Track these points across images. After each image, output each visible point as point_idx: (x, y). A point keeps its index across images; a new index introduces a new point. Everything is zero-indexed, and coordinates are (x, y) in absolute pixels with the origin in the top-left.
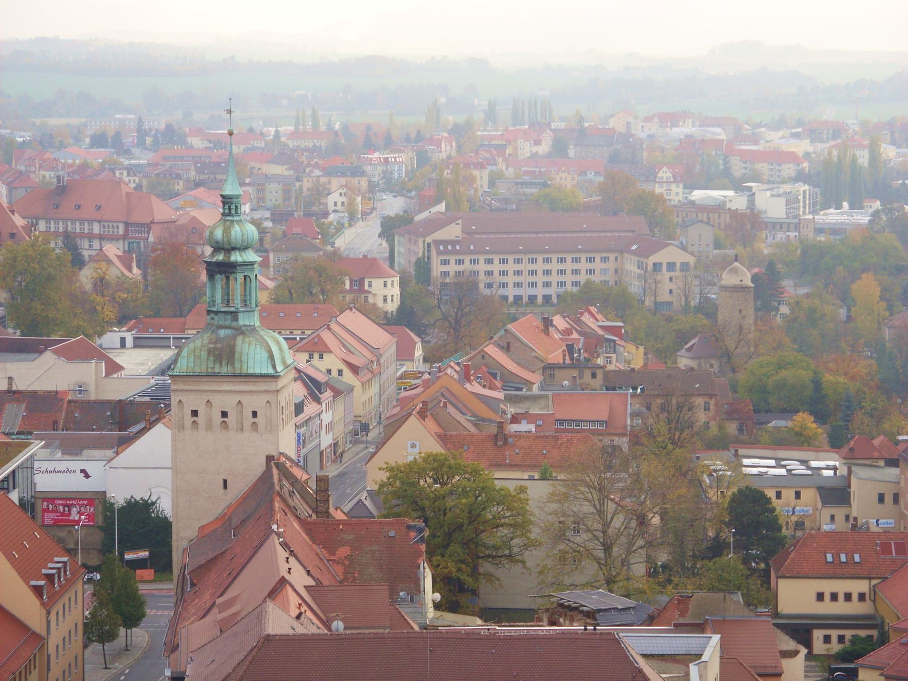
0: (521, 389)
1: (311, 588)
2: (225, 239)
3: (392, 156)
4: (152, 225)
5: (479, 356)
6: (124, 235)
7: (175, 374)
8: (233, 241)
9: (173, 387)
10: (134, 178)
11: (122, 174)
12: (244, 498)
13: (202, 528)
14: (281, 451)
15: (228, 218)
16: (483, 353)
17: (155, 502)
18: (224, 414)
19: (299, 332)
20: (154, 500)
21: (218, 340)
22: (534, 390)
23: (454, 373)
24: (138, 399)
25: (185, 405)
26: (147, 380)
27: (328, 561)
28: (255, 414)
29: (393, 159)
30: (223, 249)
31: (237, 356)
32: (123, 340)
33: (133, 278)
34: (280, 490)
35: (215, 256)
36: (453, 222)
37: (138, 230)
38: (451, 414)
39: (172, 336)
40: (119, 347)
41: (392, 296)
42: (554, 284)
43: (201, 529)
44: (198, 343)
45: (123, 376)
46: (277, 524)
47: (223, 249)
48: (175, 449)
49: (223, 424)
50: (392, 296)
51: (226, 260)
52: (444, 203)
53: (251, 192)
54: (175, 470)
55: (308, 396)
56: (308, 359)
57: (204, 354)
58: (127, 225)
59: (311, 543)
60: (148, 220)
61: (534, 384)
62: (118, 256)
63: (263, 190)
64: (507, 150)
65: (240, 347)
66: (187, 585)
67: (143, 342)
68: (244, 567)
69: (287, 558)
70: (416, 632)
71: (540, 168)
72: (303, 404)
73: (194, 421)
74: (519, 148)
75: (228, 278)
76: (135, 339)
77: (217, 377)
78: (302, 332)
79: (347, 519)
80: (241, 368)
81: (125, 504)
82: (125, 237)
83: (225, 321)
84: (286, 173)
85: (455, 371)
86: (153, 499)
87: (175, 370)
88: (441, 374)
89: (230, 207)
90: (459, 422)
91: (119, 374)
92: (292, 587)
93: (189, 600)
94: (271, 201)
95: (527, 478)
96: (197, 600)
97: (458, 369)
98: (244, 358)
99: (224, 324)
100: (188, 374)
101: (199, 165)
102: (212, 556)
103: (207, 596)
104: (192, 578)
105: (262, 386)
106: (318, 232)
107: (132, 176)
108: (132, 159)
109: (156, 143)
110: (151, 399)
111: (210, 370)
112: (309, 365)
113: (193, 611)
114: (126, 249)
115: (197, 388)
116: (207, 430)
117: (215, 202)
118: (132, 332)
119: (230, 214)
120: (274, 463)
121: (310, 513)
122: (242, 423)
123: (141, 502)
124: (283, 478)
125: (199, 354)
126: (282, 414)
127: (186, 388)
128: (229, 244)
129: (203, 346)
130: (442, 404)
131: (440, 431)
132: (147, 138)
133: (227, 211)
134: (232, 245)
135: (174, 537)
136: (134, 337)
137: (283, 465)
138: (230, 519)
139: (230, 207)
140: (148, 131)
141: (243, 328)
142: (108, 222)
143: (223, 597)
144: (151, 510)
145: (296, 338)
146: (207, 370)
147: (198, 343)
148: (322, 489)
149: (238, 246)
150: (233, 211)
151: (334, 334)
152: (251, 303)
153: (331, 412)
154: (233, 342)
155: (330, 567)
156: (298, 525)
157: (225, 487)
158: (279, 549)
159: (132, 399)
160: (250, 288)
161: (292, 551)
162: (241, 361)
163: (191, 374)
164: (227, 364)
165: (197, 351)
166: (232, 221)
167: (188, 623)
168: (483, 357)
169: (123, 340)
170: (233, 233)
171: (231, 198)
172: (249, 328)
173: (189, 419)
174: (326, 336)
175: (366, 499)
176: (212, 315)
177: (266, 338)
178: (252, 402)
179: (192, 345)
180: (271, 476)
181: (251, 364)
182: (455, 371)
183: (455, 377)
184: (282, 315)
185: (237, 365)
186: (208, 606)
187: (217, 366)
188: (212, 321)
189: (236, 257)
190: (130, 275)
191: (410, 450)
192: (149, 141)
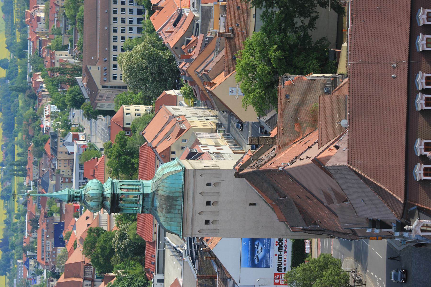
0: (198, 24)
2: (97, 200)
3: (45, 113)
5: (176, 50)
6: (92, 281)
9: (190, 236)
13: (280, 219)
15: (83, 198)
16: (174, 48)
18: (208, 203)
21: (161, 206)
22: (199, 16)
23: (186, 66)
28: (209, 184)
29: (47, 112)
30: (102, 202)
31: (171, 195)
35: (107, 207)
36: (89, 71)
38: (212, 67)
39: (157, 250)
41: (135, 110)
42: (131, 7)
43: (281, 220)
45: (182, 279)
49: (214, 204)
50: (135, 110)
52: (76, 78)
57: (170, 215)
61: (194, 16)
64: (43, 39)
66: (315, 227)
67: (161, 270)
69: (300, 159)
70: (349, 80)
71: (55, 18)
73: (212, 222)
74: (42, 31)
75: (121, 200)
76: (158, 273)
79: (277, 128)
80: (179, 192)
83: (148, 202)
85: (185, 65)
87: (179, 234)
88: (187, 74)
90: (218, 62)
95: (254, 19)
97: (184, 63)
98: (173, 190)
99: (150, 203)
101: (48, 236)
106: (93, 158)
111: (180, 212)
114: (101, 280)
117: (71, 226)
118: (154, 275)
120: (240, 172)
121: (272, 149)
125: (170, 219)
126: (209, 167)
127: (190, 228)
128: (99, 197)
130: (206, 73)
131: (223, 74)
133: (78, 199)
134: (101, 195)
138: (275, 201)
139: (76, 197)
143: (324, 202)
146: (179, 214)
148: (258, 141)
150: (79, 194)
151: (158, 144)
153: (208, 147)
156: (280, 156)
157: (255, 204)
158: (295, 165)
160: (128, 185)
162: (174, 192)
164: (176, 201)
168: (176, 48)
174: (160, 150)
175: (265, 119)
176: (145, 210)
177: (160, 176)
178: (201, 186)
180: (248, 173)
181: (176, 186)
182: (185, 65)
183: (189, 65)
185: (177, 194)
186: (328, 212)
187: (177, 207)
188: (149, 210)
191: (235, 93)
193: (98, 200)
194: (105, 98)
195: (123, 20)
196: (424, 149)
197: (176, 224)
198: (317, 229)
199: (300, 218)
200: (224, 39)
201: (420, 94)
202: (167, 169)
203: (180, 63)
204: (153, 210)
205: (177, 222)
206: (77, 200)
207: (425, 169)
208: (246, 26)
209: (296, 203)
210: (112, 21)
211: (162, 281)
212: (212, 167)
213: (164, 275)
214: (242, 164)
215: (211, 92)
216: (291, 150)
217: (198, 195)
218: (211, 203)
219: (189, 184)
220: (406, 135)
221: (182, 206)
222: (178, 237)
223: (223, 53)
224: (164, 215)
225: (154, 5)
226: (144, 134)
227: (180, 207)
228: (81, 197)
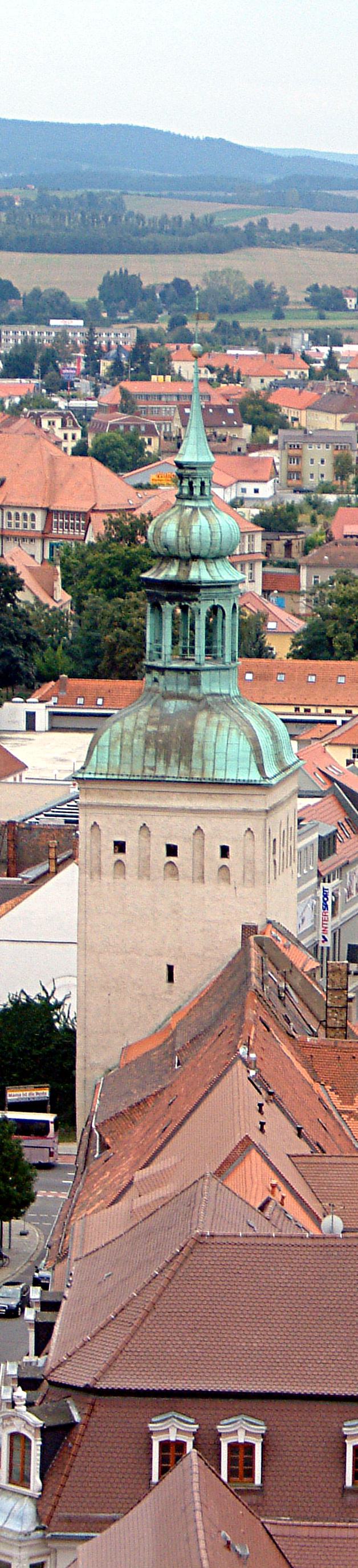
1: (300, 1160)
2: (180, 540)
4: (93, 516)
6: (43, 533)
7: (86, 776)
8: (195, 544)
10: (74, 432)
11: (52, 424)
12: (200, 999)
14: (269, 918)
15: (187, 503)
17: (62, 1003)
18: (172, 850)
19: (342, 711)
20: (60, 1000)
21: (165, 719)
24: (44, 820)
25: (104, 832)
26: (66, 788)
27: (340, 1113)
28: (225, 851)
30: (178, 557)
31: (196, 747)
32: (31, 717)
33: (55, 609)
34: (259, 987)
35: (162, 570)
37: (73, 524)
40: (24, 728)
44: (129, 723)
46: (248, 1045)
47: (178, 557)
48: (83, 910)
49: (169, 867)
51: (182, 578)
53: (277, 460)
54: (83, 945)
55: (345, 824)
56: (351, 757)
57: (138, 743)
58: (49, 512)
59: (310, 1080)
60: (86, 507)
62: (30, 569)
63: (299, 458)
65: (201, 732)
67: (61, 722)
68: (187, 1117)
69: (261, 1105)
72: (335, 837)
76: (53, 715)
77: (161, 784)
78: (347, 712)
80: (203, 770)
81: (9, 1006)
82: (44, 536)
84: (341, 427)
86: (59, 997)
87: (88, 770)
89: (191, 484)
91: (18, 776)
92: (264, 1156)
93: (96, 1174)
94: (312, 476)
96: (108, 1173)
98: (209, 751)
100: (109, 777)
102: (138, 1099)
103: (124, 1167)
104: (104, 1135)
105: (238, 802)
107: (70, 429)
108: (74, 397)
109: (118, 371)
110: (66, 822)
111: (148, 772)
112: (350, 770)
113: (100, 1192)
114: (47, 556)
115: (122, 802)
116: (140, 877)
118: (47, 704)
119: (191, 497)
120: (255, 939)
122: (203, 867)
123: (37, 1001)
124: (270, 965)
125: (130, 744)
126: (274, 853)
127: (105, 801)
128: (189, 549)
129: (136, 728)
132: (102, 361)
133: (186, 491)
134: (194, 552)
135: (79, 1063)
136: (49, 712)
137: (271, 942)
139: (191, 484)
140: (105, 350)
141: (209, 699)
142: (18, 507)
143: (151, 1167)
144: (55, 1017)
145: (334, 722)
147: (129, 723)
148: (336, 987)
149: (203, 553)
150: (197, 492)
152: (223, 656)
154: (190, 723)
155: (342, 1124)
157: (171, 979)
159: (33, 820)
160: (223, 627)
161: (271, 1094)
163: (116, 777)
164: (179, 762)
165: (127, 737)
166: (195, 509)
167: (91, 1211)
169: (31, 717)
170: (195, 529)
171: (194, 468)
172: (219, 699)
173: (109, 856)
179: (117, 727)
181: (220, 762)
184: (312, 679)
185: (196, 764)
187: (161, 764)
188: (155, 685)
189: (198, 573)
190: (52, 604)
192: (105, 365)
193: (180, 546)
196: (237, 1443)
198: (92, 1151)
202: (268, 735)
204: (155, 698)
205: (120, 763)
206: (181, 487)
207: (250, 1448)
211: (31, 726)
212: (275, 861)
213: (46, 731)
214: (280, 944)
216: (304, 1080)
217: (196, 821)
218: (172, 859)
219: (226, 797)
220: (276, 1393)
221: (163, 777)
222: (78, 767)
224: (140, 729)
227: (163, 773)
228: (190, 499)
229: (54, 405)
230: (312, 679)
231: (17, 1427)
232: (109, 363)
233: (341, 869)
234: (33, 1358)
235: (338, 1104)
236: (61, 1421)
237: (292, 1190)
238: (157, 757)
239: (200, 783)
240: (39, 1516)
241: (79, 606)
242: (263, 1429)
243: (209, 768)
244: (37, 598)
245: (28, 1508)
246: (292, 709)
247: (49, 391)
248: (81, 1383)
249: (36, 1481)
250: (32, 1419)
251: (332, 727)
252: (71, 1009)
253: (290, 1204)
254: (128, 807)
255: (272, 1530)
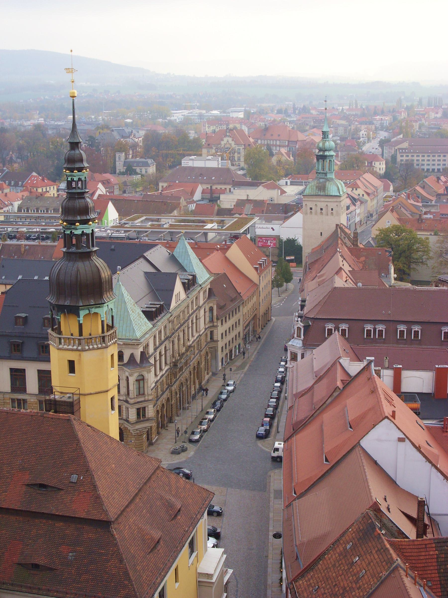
0: (428, 203)
8: (326, 147)
18: (321, 209)
19: (349, 181)
21: (320, 183)
23: (404, 196)
24: (292, 203)
27: (357, 262)
28: (332, 209)
31: (326, 189)
32: (287, 182)
48: (304, 221)
51: (323, 154)
54: (304, 228)
58: (289, 141)
60: (296, 140)
63: (337, 129)
75: (324, 161)
82: (288, 146)
97: (405, 195)
98: (329, 189)
102: (316, 259)
105: (334, 200)
109: (299, 112)
111: (317, 194)
115: (312, 200)
119: (325, 138)
129: (314, 185)
131: (398, 217)
133: (324, 137)
138: (323, 246)
147: (313, 184)
149: (327, 149)
150: (326, 137)
151: (361, 181)
157: (321, 235)
158: (340, 257)
165: (312, 186)
169: (287, 182)
173: (309, 211)
174: (358, 182)
176: (318, 174)
177: (337, 182)
180: (338, 232)
181: (331, 192)
184: (343, 174)
185: (326, 192)
187: (319, 192)
189: (327, 153)
192: (297, 112)
194: (390, 151)
195: (434, 160)
197: (310, 191)
199: (313, 260)
200: (418, 217)
201: (373, 327)
203: (406, 193)
208: (425, 230)
209: (320, 258)
210: (412, 154)
215: (388, 211)
217: (326, 203)
223: (410, 217)
225: (440, 178)
226: (367, 173)
229: (287, 120)
230: (343, 174)
231: (299, 326)
232: (298, 111)
233: (351, 212)
234: (300, 312)
235: (356, 260)
236: (307, 325)
237: (350, 277)
238: (318, 191)
239: (327, 196)
240: (303, 344)
241: (295, 160)
242: (385, 327)
243: (329, 192)
244: (287, 159)
245: (301, 342)
246: (345, 180)
247: (286, 117)
248: (311, 317)
249: (302, 337)
250: (302, 324)
251: (347, 184)
252: (300, 241)
253: (350, 280)
254: (313, 201)
255: (352, 347)
